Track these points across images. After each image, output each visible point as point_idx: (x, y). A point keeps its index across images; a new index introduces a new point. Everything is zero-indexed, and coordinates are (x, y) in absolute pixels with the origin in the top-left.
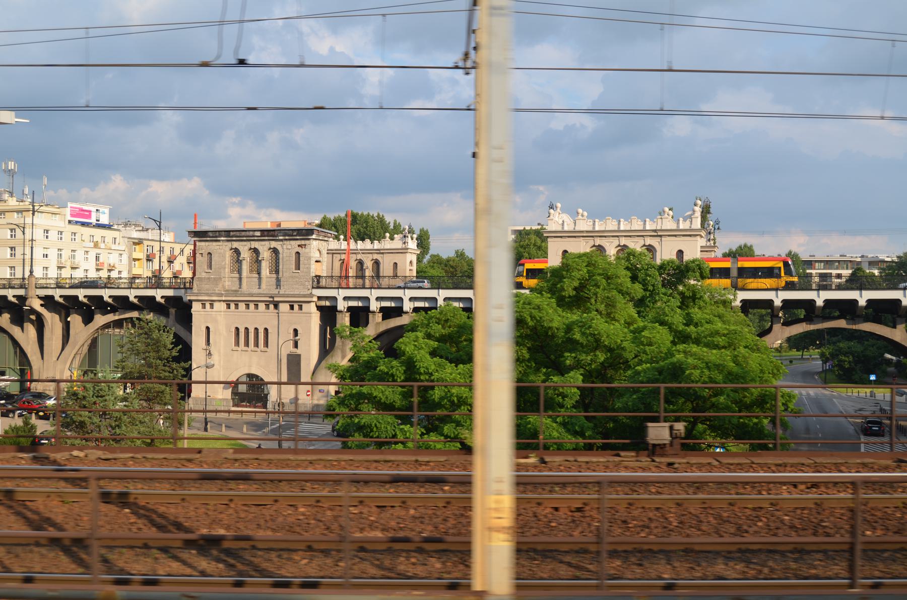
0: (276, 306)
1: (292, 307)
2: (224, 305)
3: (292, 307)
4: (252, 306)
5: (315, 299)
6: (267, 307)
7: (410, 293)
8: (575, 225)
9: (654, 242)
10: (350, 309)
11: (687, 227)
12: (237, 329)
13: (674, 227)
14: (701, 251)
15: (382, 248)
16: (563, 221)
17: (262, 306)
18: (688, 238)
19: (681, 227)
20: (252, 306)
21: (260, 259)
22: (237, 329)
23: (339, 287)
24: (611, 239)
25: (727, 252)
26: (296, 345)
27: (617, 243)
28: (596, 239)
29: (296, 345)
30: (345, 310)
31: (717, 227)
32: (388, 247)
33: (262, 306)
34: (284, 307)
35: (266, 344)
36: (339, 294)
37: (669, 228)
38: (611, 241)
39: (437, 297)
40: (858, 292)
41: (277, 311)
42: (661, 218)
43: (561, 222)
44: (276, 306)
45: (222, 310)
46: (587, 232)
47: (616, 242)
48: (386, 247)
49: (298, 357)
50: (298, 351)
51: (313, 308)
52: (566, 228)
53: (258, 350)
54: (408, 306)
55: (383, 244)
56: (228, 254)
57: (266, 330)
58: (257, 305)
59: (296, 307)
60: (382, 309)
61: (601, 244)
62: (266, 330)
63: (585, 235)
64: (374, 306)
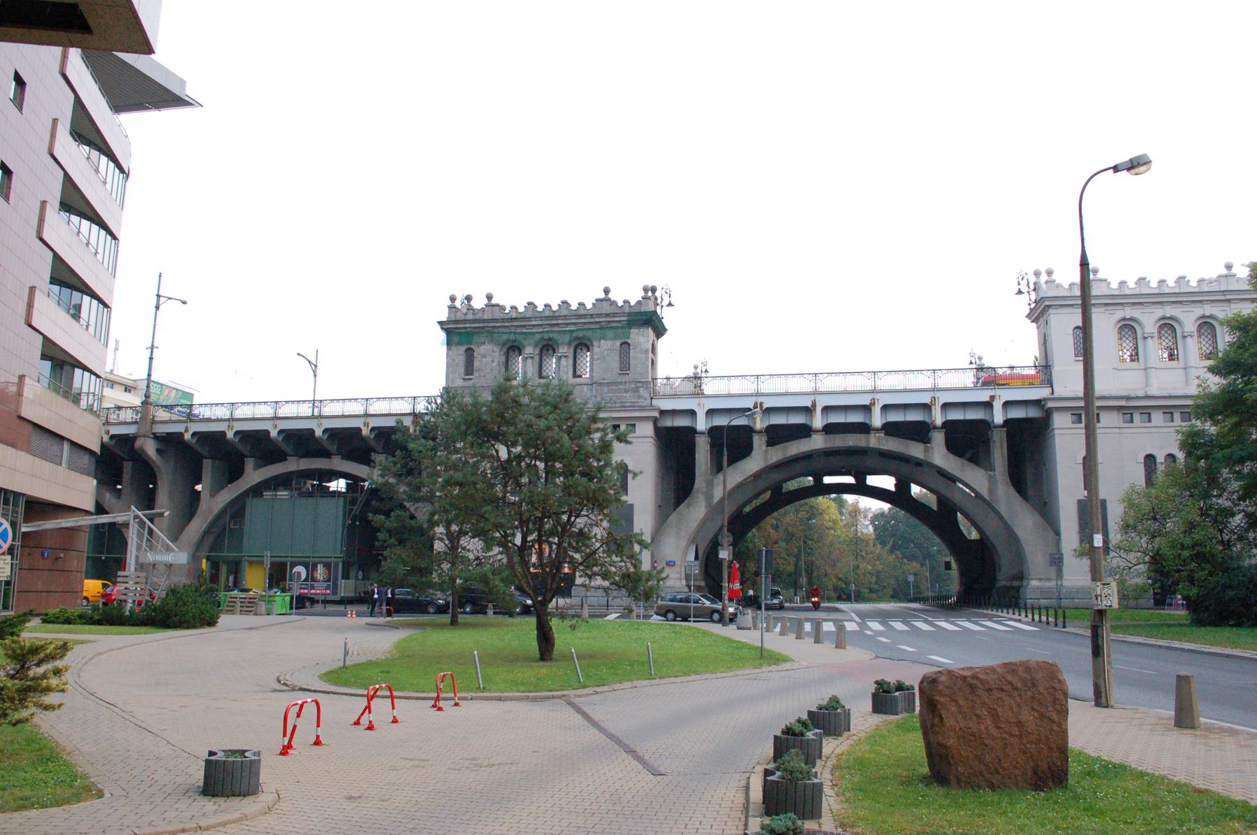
38: (1152, 311)
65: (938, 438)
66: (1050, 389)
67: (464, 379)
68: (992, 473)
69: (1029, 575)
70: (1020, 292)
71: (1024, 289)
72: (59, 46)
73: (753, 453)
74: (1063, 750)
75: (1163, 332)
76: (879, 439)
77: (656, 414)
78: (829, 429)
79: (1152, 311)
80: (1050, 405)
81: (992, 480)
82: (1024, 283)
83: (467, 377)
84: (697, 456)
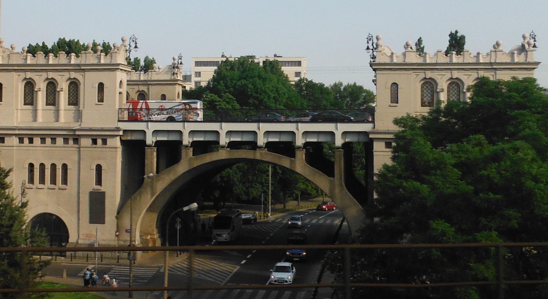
0: (76, 140)
1: (95, 142)
2: (16, 140)
3: (95, 142)
4: (48, 140)
5: (121, 133)
6: (66, 141)
7: (153, 127)
8: (405, 58)
9: (77, 76)
10: (158, 144)
11: (108, 62)
12: (31, 166)
13: (96, 62)
14: (127, 84)
15: (149, 79)
16: (392, 54)
17: (60, 141)
18: (405, 72)
19: (516, 60)
20: (48, 140)
21: (438, 90)
22: (31, 166)
23: (185, 121)
24: (443, 73)
25: (325, 86)
26: (99, 181)
27: (450, 76)
28: (427, 72)
29: (99, 181)
30: (153, 145)
31: (180, 61)
32: (156, 79)
33: (60, 141)
34: (86, 142)
35: (65, 181)
36: (222, 129)
37: (504, 61)
38: (470, 74)
39: (296, 131)
40: (218, 124)
41: (76, 146)
42: (495, 51)
43: (389, 54)
44: (76, 140)
45: (15, 145)
46: (18, 65)
47: (448, 75)
48: (153, 79)
49: (103, 194)
50: (102, 189)
51: (117, 142)
52: (395, 61)
53: (56, 187)
54: (224, 140)
55: (150, 75)
56: (21, 87)
57: (65, 167)
58: (96, 139)
59: (99, 141)
60: (194, 144)
61: (76, 77)
62: (65, 167)
63: (416, 67)
64: (187, 140)
65: (301, 155)
66: (373, 124)
67: (390, 106)
68: (332, 179)
69: (54, 113)
70: (368, 48)
71: (371, 47)
72: (186, 211)
73: (182, 161)
74: (73, 140)
75: (72, 87)
76: (261, 154)
77: (121, 133)
78: (233, 145)
79: (470, 74)
80: (371, 136)
81: (332, 184)
82: (371, 42)
83: (392, 104)
84: (146, 161)
